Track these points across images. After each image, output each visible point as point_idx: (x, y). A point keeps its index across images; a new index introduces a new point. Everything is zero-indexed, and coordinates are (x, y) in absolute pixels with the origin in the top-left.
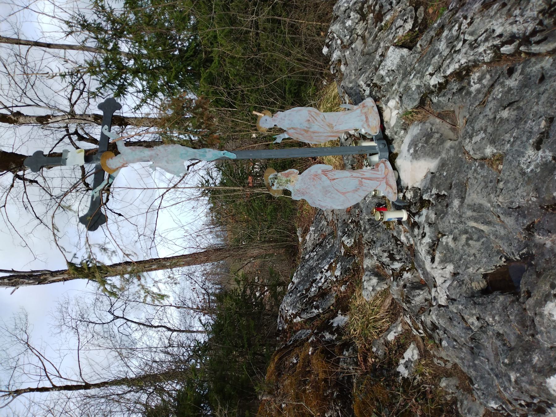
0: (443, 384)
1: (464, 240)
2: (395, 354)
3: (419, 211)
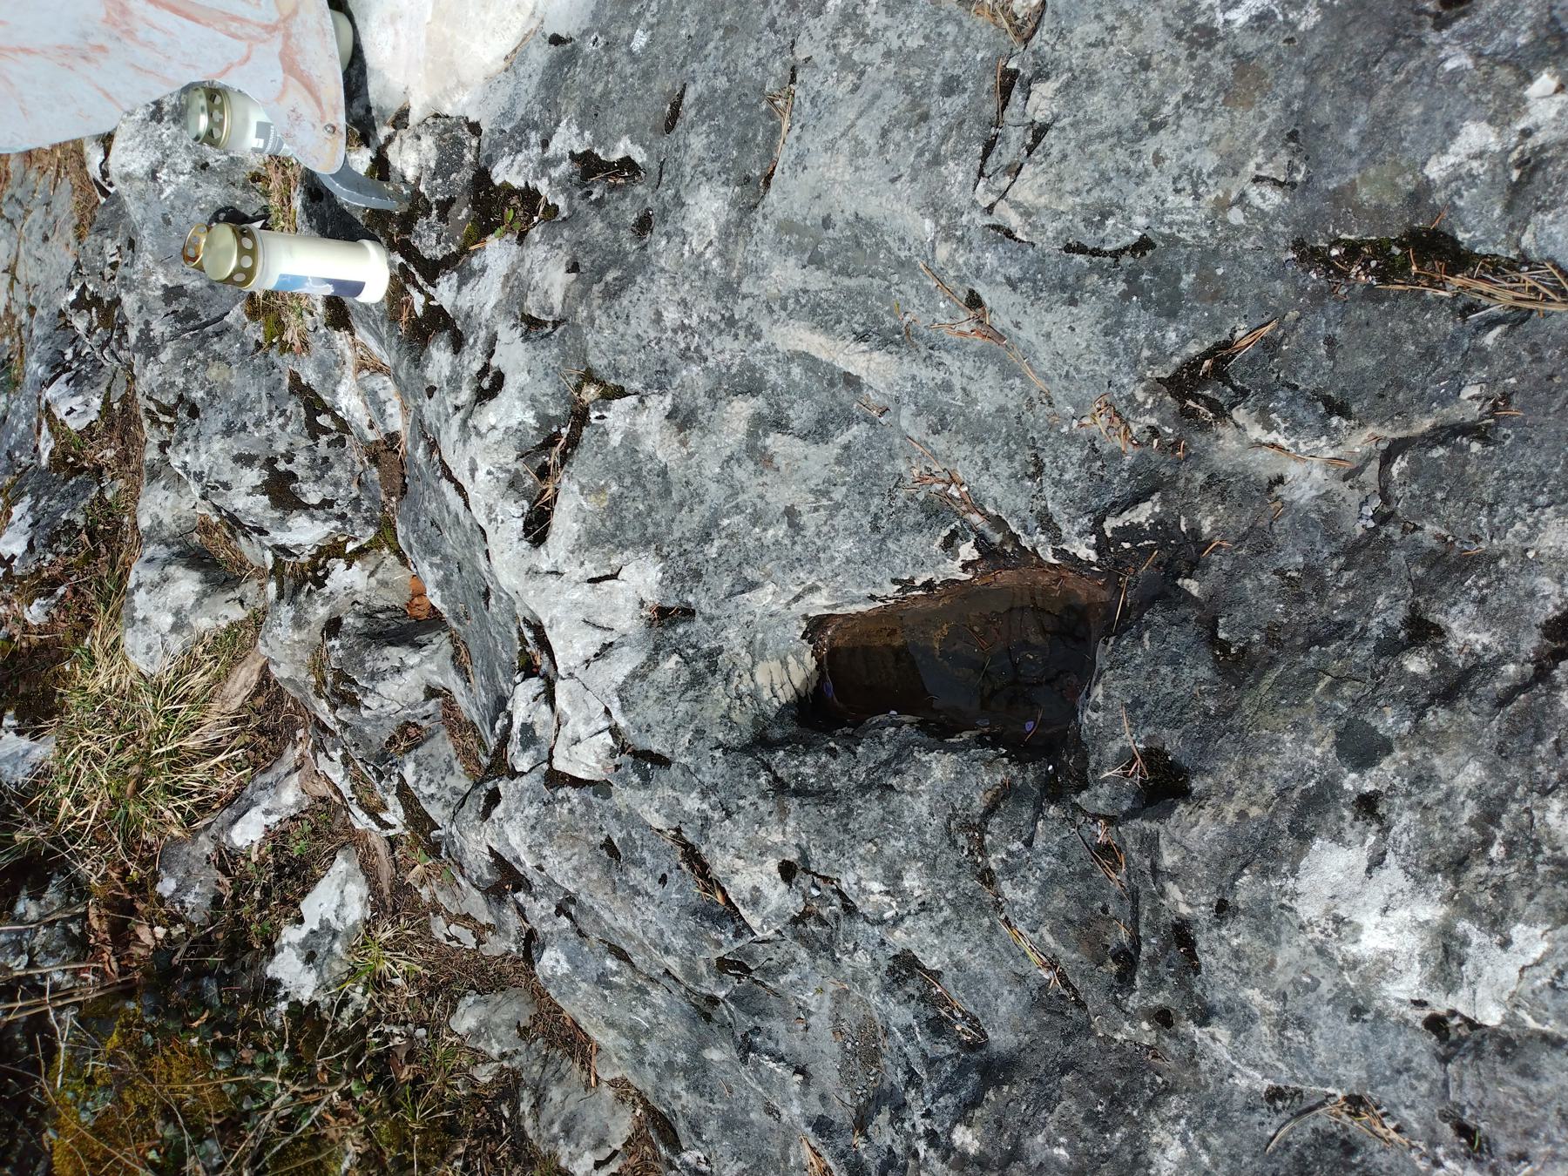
0: (466, 1020)
1: (743, 427)
2: (262, 905)
3: (464, 250)
